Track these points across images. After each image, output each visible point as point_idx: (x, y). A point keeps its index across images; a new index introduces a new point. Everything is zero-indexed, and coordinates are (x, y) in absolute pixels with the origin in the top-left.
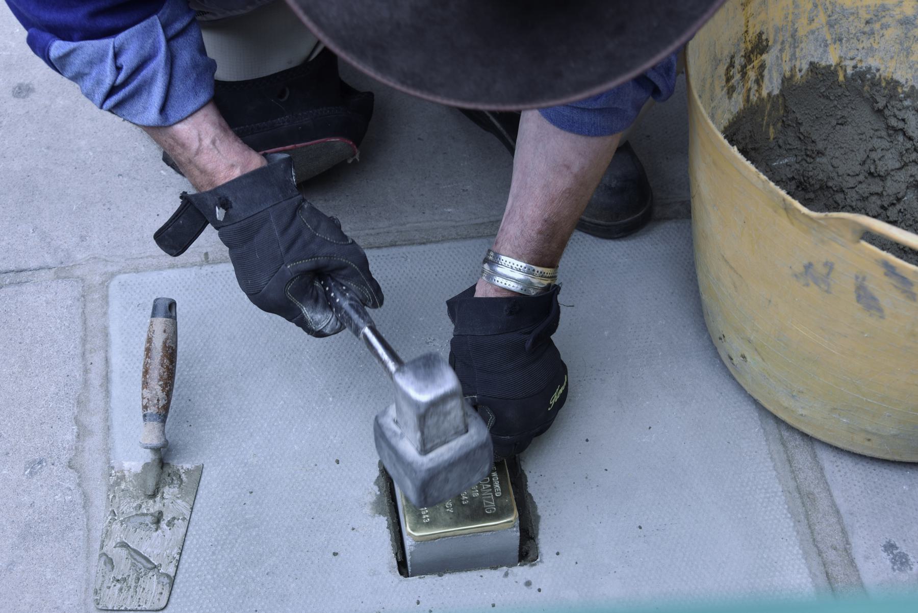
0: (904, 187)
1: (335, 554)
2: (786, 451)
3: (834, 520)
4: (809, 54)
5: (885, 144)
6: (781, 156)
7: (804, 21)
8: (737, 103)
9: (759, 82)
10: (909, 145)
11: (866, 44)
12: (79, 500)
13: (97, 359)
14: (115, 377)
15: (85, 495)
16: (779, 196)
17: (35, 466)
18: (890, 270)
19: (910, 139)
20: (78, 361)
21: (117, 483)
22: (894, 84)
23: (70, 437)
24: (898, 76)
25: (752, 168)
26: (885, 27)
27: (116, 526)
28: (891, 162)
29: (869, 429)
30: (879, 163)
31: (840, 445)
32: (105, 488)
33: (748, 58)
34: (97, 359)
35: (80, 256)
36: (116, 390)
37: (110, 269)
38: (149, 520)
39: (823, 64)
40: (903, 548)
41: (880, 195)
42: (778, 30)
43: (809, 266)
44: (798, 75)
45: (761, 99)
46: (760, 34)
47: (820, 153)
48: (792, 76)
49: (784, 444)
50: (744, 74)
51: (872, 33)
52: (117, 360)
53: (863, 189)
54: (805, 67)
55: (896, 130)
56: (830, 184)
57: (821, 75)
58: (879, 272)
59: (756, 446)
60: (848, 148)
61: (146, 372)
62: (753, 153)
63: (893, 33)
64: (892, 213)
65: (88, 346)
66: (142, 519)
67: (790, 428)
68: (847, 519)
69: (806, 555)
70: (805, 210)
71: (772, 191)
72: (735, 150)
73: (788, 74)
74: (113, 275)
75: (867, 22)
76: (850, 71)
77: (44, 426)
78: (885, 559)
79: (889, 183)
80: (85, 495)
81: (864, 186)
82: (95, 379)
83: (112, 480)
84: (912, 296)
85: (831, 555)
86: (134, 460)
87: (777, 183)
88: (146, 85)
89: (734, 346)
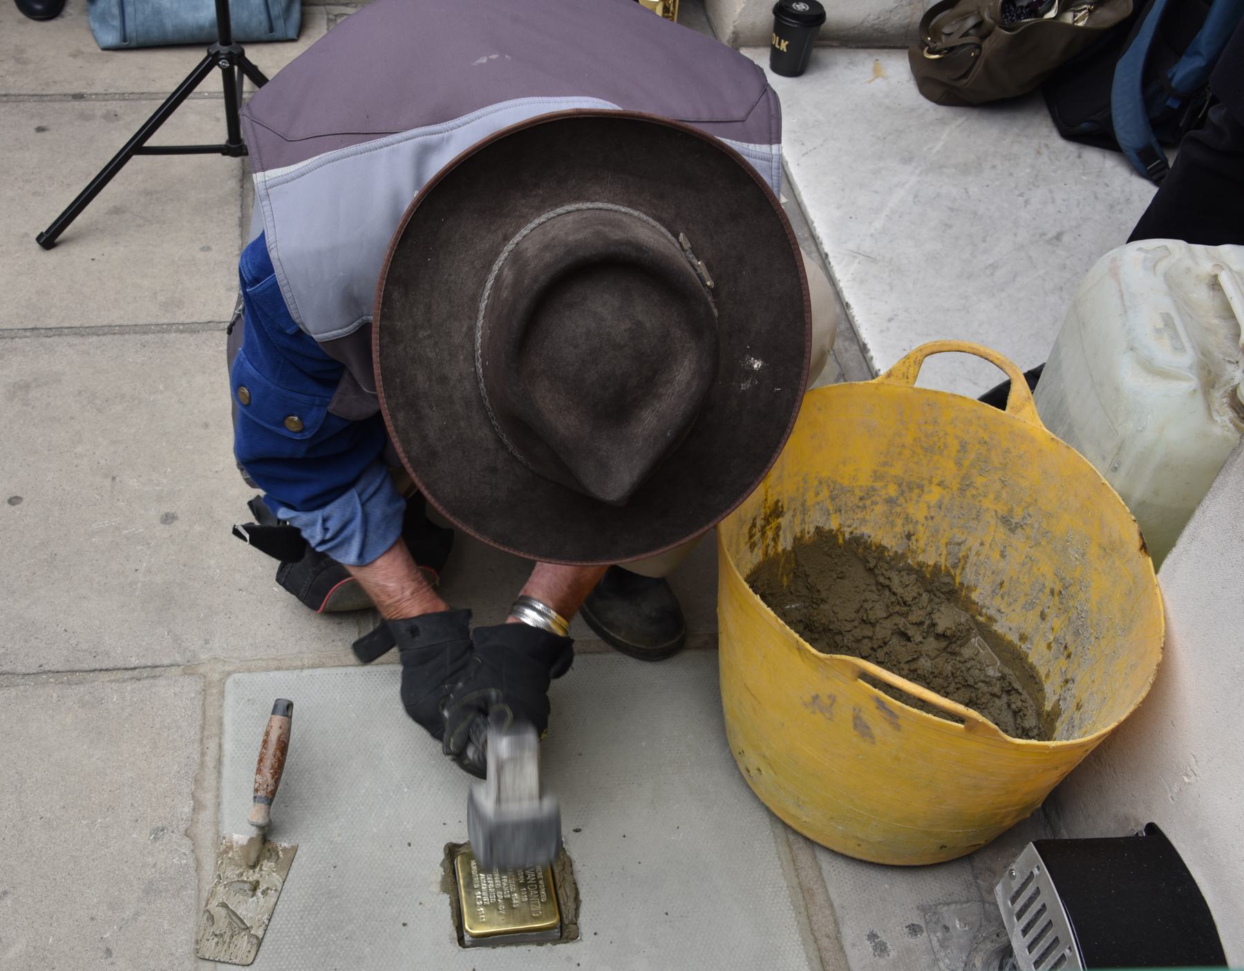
0: (889, 633)
1: (404, 925)
2: (791, 851)
3: (828, 912)
4: (815, 520)
5: (875, 597)
6: (792, 601)
7: (811, 494)
8: (757, 556)
9: (776, 539)
10: (893, 599)
11: (860, 515)
12: (192, 864)
14: (226, 761)
15: (198, 861)
16: (793, 638)
17: (158, 832)
18: (881, 704)
19: (894, 594)
20: (196, 745)
21: (226, 852)
22: (882, 549)
24: (885, 543)
25: (772, 613)
26: (874, 503)
27: (220, 889)
28: (879, 612)
29: (860, 835)
30: (870, 613)
31: (836, 849)
32: (214, 856)
33: (767, 521)
34: (212, 745)
35: (203, 657)
36: (227, 772)
37: (228, 668)
38: (247, 887)
39: (827, 528)
40: (883, 937)
41: (871, 638)
42: (792, 499)
43: (816, 698)
44: (807, 536)
45: (777, 554)
46: (778, 501)
47: (823, 601)
48: (802, 537)
49: (790, 846)
50: (763, 533)
51: (864, 507)
52: (228, 746)
53: (858, 633)
54: (812, 530)
56: (831, 627)
57: (825, 537)
59: (767, 859)
60: (845, 600)
61: (261, 761)
62: (770, 598)
63: (880, 508)
64: (880, 654)
65: (206, 733)
66: (241, 885)
68: (839, 912)
70: (814, 651)
72: (758, 597)
73: (799, 535)
74: (229, 674)
75: (861, 499)
76: (847, 536)
77: (168, 800)
78: (869, 946)
79: (878, 628)
80: (198, 861)
81: (858, 630)
82: (210, 762)
83: (222, 848)
84: (898, 727)
85: (825, 942)
86: (241, 835)
87: (789, 623)
88: (348, 540)
89: (751, 760)
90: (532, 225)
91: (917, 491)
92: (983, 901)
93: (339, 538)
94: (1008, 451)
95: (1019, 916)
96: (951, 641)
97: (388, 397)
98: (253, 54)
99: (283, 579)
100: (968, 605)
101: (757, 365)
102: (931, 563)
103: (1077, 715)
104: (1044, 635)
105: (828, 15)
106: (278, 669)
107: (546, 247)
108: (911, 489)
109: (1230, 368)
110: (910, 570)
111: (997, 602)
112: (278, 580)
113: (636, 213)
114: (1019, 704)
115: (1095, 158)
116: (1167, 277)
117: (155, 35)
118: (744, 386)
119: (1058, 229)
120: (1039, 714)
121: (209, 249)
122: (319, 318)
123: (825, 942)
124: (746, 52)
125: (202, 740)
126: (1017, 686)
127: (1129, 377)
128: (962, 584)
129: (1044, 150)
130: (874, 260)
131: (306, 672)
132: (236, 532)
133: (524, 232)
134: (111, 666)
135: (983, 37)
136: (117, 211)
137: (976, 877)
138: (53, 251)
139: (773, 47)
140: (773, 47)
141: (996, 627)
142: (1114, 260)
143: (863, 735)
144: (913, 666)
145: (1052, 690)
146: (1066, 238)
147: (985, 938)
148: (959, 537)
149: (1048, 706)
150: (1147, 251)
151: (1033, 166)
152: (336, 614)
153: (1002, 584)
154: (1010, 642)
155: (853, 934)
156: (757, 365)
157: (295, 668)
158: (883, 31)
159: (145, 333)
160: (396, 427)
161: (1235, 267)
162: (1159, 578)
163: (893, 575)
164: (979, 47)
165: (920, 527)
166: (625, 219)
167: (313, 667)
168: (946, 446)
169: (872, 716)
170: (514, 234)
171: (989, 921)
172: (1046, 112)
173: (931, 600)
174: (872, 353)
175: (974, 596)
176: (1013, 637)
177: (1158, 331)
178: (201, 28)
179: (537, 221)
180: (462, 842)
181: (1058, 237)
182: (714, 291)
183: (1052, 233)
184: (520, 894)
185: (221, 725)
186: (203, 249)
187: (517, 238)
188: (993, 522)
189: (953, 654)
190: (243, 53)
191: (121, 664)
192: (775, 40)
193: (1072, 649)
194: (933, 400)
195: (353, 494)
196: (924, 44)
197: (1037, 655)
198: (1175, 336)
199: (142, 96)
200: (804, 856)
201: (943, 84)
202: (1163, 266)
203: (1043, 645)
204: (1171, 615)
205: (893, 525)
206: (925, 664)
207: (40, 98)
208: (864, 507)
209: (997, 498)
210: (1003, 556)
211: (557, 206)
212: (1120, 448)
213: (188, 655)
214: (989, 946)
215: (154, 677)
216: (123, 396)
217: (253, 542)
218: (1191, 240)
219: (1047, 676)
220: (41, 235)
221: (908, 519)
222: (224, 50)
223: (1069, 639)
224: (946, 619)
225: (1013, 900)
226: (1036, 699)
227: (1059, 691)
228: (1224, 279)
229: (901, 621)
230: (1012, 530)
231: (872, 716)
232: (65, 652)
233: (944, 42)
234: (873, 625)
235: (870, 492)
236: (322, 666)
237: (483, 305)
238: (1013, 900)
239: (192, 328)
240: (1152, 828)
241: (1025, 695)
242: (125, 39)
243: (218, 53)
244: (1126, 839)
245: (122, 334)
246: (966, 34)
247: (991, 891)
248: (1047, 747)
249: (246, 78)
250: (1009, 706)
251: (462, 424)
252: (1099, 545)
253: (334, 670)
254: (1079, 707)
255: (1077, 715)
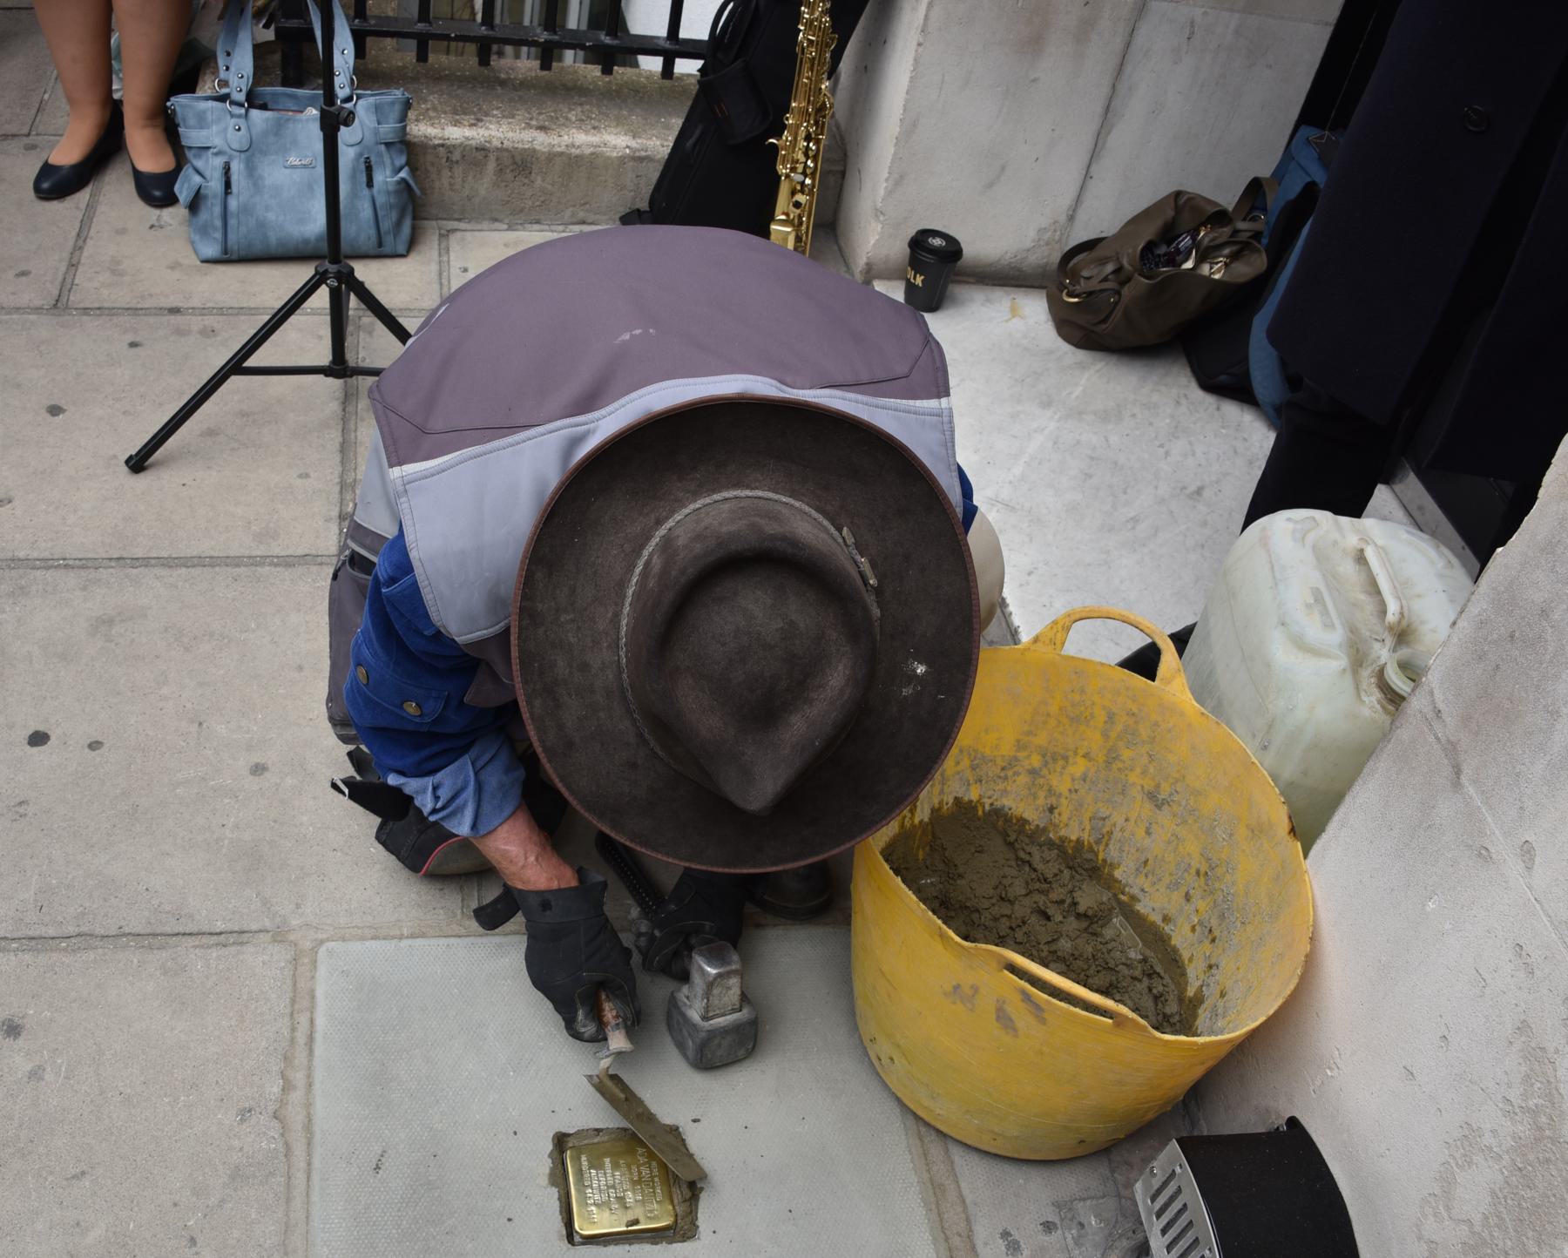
5: (1014, 872)
6: (927, 876)
13: (303, 1019)
14: (318, 1037)
15: (287, 1145)
17: (245, 1113)
18: (1027, 997)
20: (287, 1019)
22: (1023, 822)
23: (276, 1089)
24: (1026, 816)
25: (914, 898)
26: (1017, 774)
28: (1018, 889)
34: (303, 1019)
35: (295, 922)
36: (319, 1050)
37: (320, 936)
40: (1016, 1235)
41: (1009, 917)
43: (957, 987)
45: (913, 825)
47: (961, 876)
48: (939, 809)
51: (1006, 778)
52: (321, 1021)
53: (996, 911)
54: (951, 801)
55: (1024, 862)
58: (1016, 998)
59: (897, 1142)
67: (927, 1124)
69: (935, 1241)
70: (958, 939)
71: (929, 920)
72: (887, 867)
74: (322, 942)
76: (987, 807)
77: (256, 1078)
78: (1001, 1244)
79: (1016, 907)
80: (287, 1145)
82: (301, 1039)
84: (1043, 1021)
85: (956, 1241)
87: (924, 900)
88: (461, 809)
89: (883, 1048)
90: (686, 511)
91: (1061, 762)
92: (1119, 1196)
93: (451, 805)
94: (1156, 724)
95: (1158, 1217)
96: (1092, 921)
97: (525, 682)
98: (364, 271)
99: (383, 837)
100: (1110, 883)
101: (921, 669)
102: (1074, 838)
103: (1221, 1003)
104: (1188, 917)
105: (965, 251)
106: (375, 938)
107: (698, 537)
108: (1055, 760)
109: (1377, 646)
110: (1051, 844)
111: (1141, 880)
112: (378, 838)
113: (797, 504)
114: (1161, 988)
115: (1233, 411)
116: (1316, 549)
117: (258, 249)
118: (905, 692)
119: (1199, 484)
120: (1181, 1000)
121: (307, 476)
122: (458, 603)
123: (956, 1241)
124: (879, 286)
125: (292, 1014)
126: (1158, 969)
127: (1281, 654)
128: (1104, 861)
129: (1183, 401)
130: (1013, 509)
131: (405, 943)
132: (334, 786)
133: (678, 517)
134: (195, 930)
135: (1123, 283)
136: (211, 433)
137: (1112, 1171)
138: (142, 475)
139: (908, 281)
140: (908, 281)
141: (1139, 907)
142: (1264, 529)
143: (1005, 1027)
144: (1053, 947)
145: (1195, 974)
146: (1207, 493)
147: (1121, 1236)
148: (1104, 812)
149: (1190, 992)
150: (1296, 522)
151: (1172, 417)
152: (439, 877)
153: (1146, 862)
154: (1153, 924)
155: (984, 1231)
156: (921, 669)
157: (393, 938)
158: (1020, 270)
159: (237, 566)
160: (532, 714)
161: (1380, 542)
162: (1308, 864)
163: (1034, 850)
164: (1118, 293)
165: (1064, 802)
166: (785, 511)
167: (412, 936)
168: (1092, 715)
169: (1017, 1010)
170: (667, 518)
171: (1124, 1216)
172: (1184, 361)
173: (1072, 877)
174: (1011, 608)
175: (1117, 874)
176: (1156, 918)
177: (1308, 606)
178: (306, 242)
179: (692, 507)
180: (571, 1131)
181: (1199, 491)
182: (878, 591)
183: (1193, 488)
184: (634, 1193)
185: (313, 997)
186: (300, 476)
187: (670, 523)
188: (1139, 797)
189: (1095, 934)
190: (352, 270)
191: (206, 928)
192: (911, 274)
193: (1216, 933)
194: (1080, 668)
195: (466, 761)
196: (1062, 287)
197: (1181, 938)
198: (1325, 612)
199: (241, 311)
200: (936, 1150)
201: (1082, 328)
202: (1311, 537)
203: (1187, 928)
204: (1319, 903)
205: (1035, 797)
206: (1065, 945)
207: (134, 311)
208: (1006, 778)
209: (1144, 772)
210: (1148, 833)
211: (714, 491)
212: (1270, 727)
213: (278, 919)
214: (1125, 1243)
215: (242, 944)
216: (212, 634)
217: (351, 797)
218: (1337, 511)
219: (1191, 960)
220: (131, 457)
221: (1051, 792)
222: (333, 268)
223: (1214, 922)
224: (1089, 897)
225: (1153, 1199)
226: (1178, 984)
227: (1202, 976)
228: (1370, 554)
229: (1041, 899)
230: (1159, 807)
231: (1017, 1010)
232: (146, 914)
233: (1082, 286)
234: (1012, 903)
235: (1012, 762)
236: (423, 936)
237: (630, 592)
238: (1153, 1199)
239: (287, 562)
240: (1293, 1122)
241: (1167, 980)
242: (225, 251)
243: (326, 271)
244: (1268, 1134)
245: (212, 566)
246: (1105, 279)
247: (1129, 1185)
248: (1195, 1043)
249: (352, 296)
250: (1150, 990)
251: (602, 714)
252: (1247, 826)
253: (434, 941)
254: (1223, 995)
255: (1221, 1003)
